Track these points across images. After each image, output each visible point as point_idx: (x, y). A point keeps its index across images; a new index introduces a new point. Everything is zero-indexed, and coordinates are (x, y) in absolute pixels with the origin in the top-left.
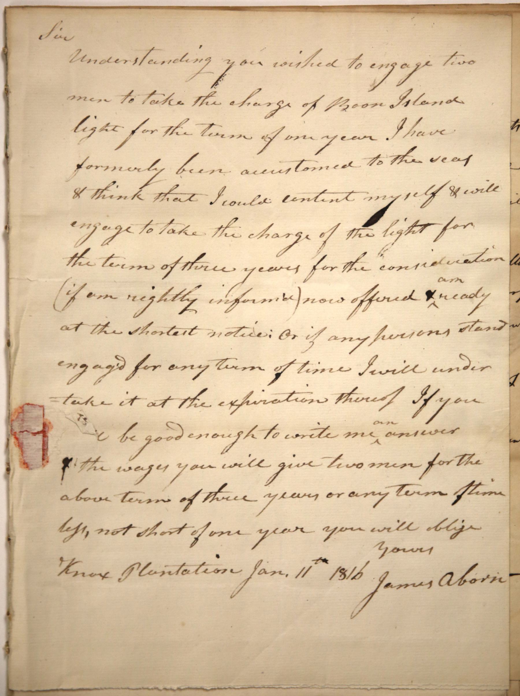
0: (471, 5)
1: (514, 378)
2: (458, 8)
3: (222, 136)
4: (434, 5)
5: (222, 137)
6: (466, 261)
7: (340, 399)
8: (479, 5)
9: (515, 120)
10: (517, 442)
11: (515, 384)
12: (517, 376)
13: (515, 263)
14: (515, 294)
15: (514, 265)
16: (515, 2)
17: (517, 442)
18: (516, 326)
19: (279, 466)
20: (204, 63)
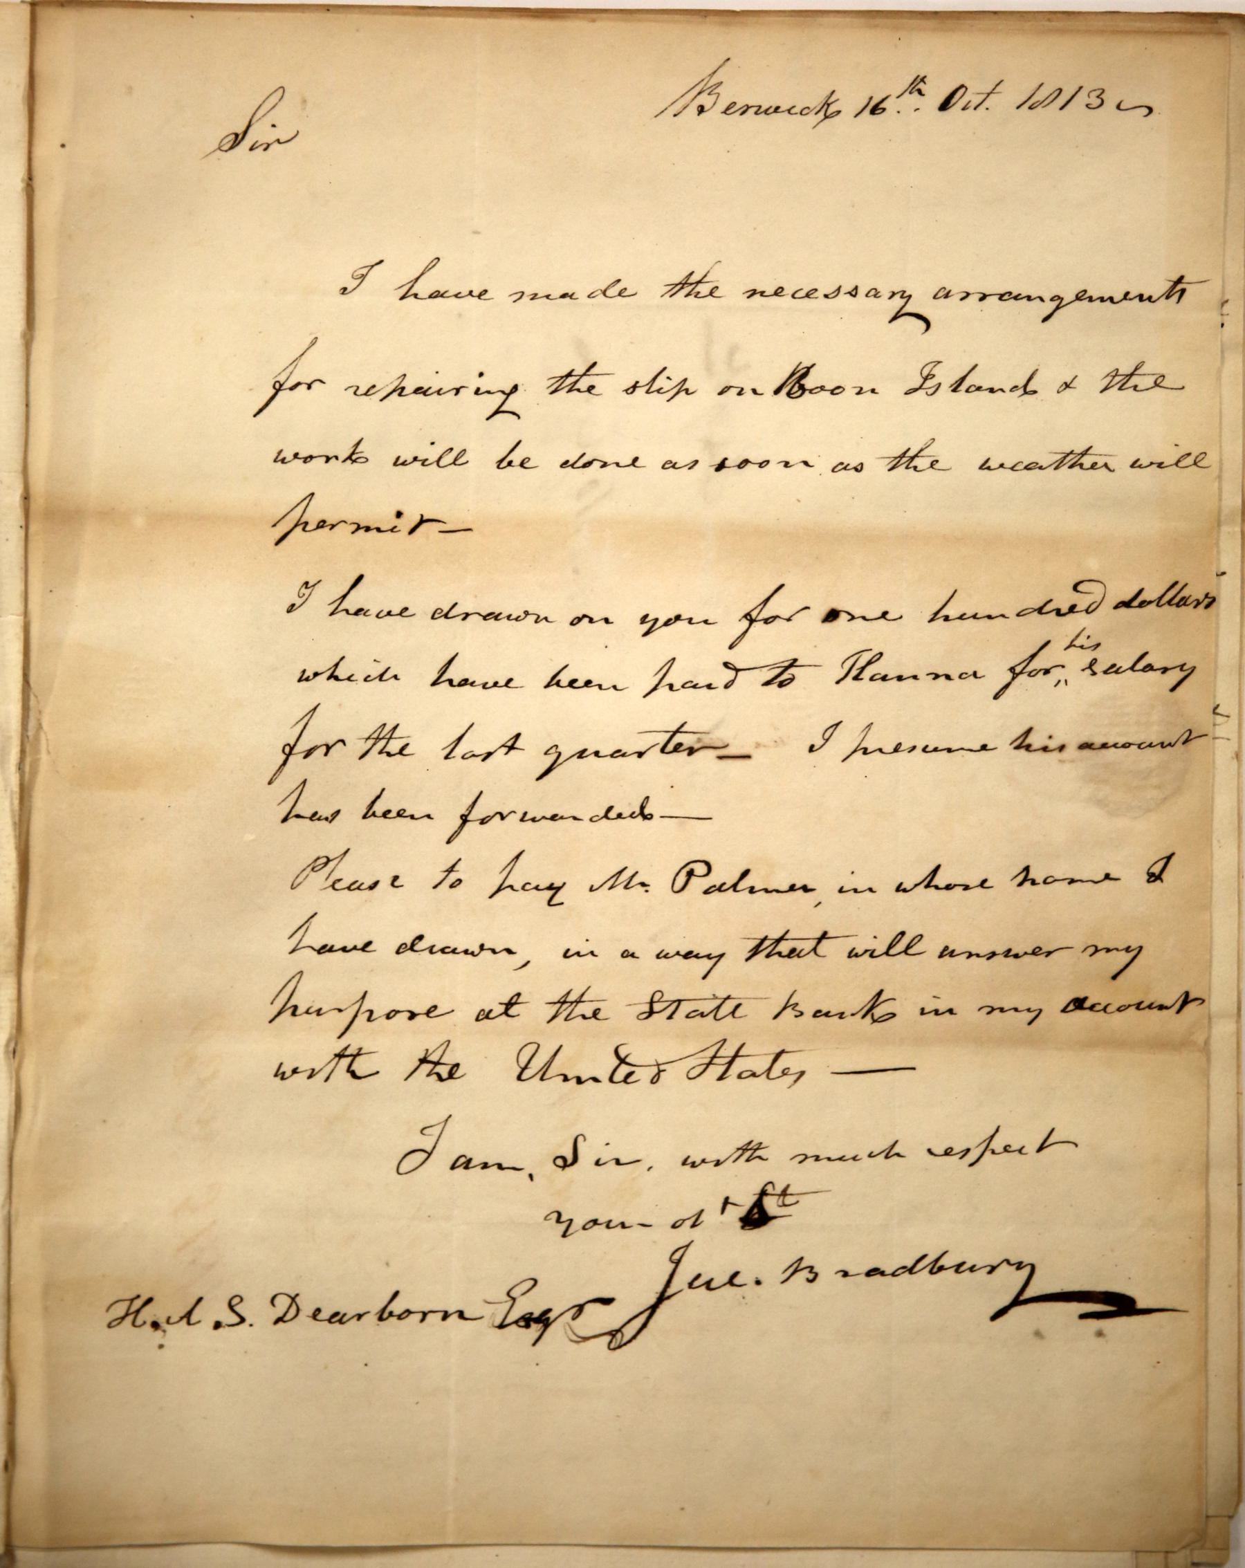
0: (1080, 13)
1: (1161, 864)
2: (1049, 20)
3: (319, 1012)
4: (995, 13)
5: (319, 1014)
6: (873, 1272)
7: (755, 951)
8: (1096, 13)
9: (1175, 278)
10: (1167, 1008)
11: (1164, 876)
12: (1169, 858)
13: (1169, 602)
14: (1169, 672)
15: (1167, 607)
16: (1179, 10)
17: (1167, 1008)
18: (1169, 744)
19: (884, 109)
20: (423, 288)
